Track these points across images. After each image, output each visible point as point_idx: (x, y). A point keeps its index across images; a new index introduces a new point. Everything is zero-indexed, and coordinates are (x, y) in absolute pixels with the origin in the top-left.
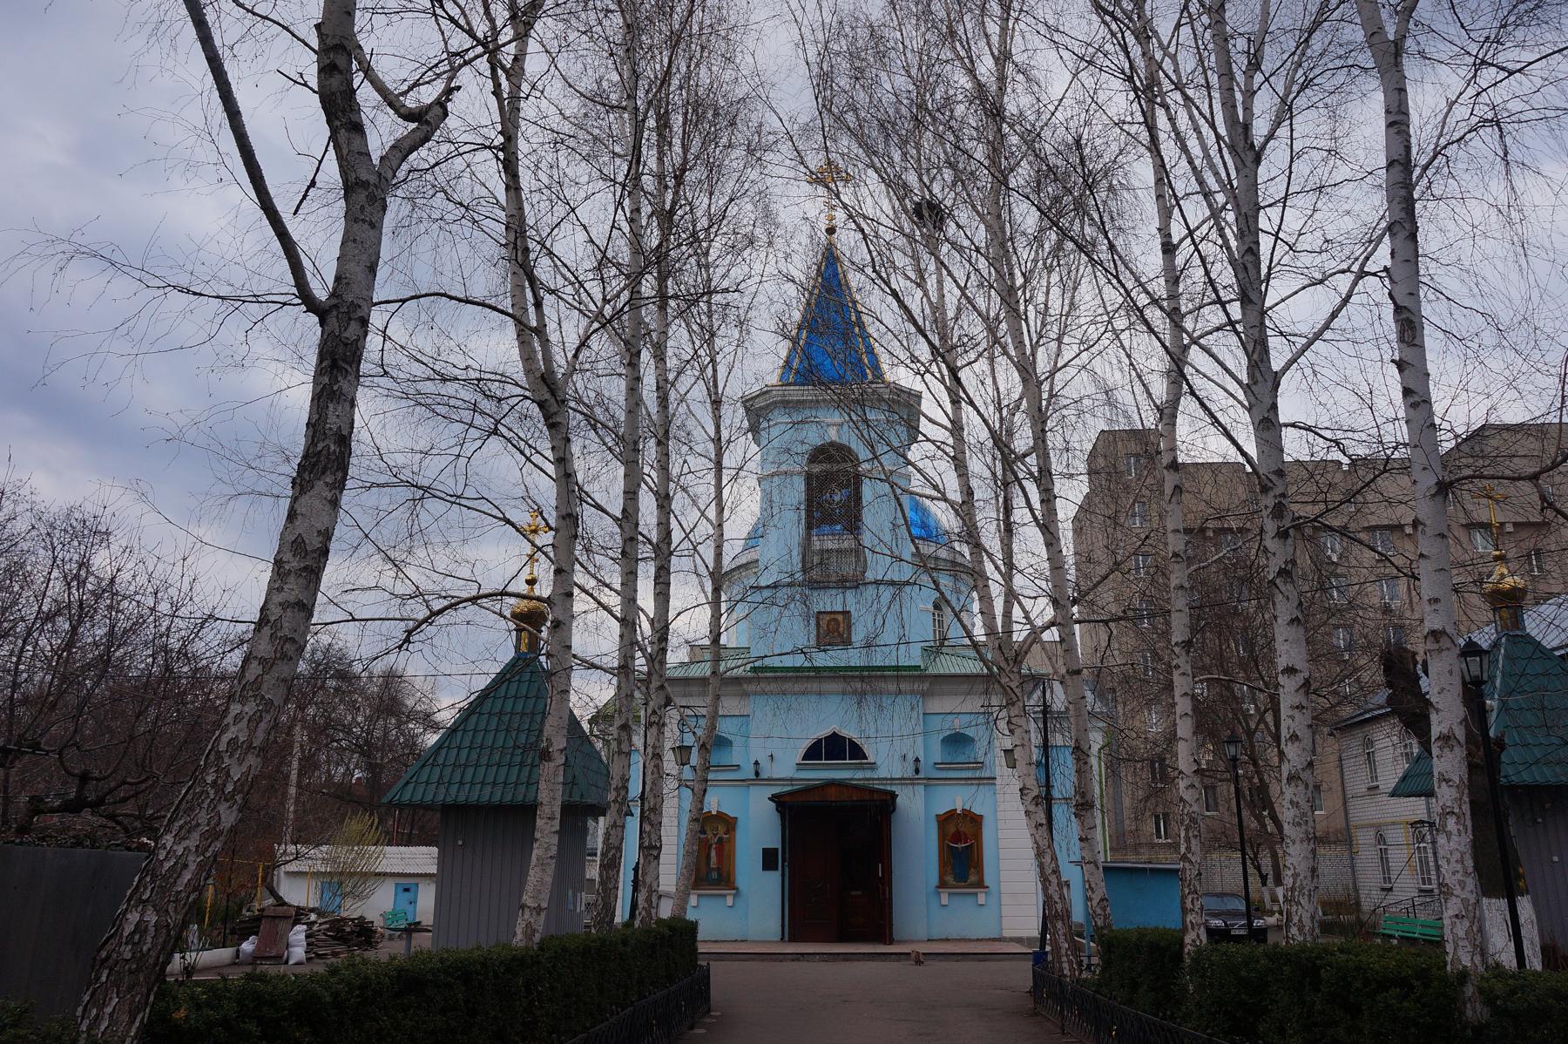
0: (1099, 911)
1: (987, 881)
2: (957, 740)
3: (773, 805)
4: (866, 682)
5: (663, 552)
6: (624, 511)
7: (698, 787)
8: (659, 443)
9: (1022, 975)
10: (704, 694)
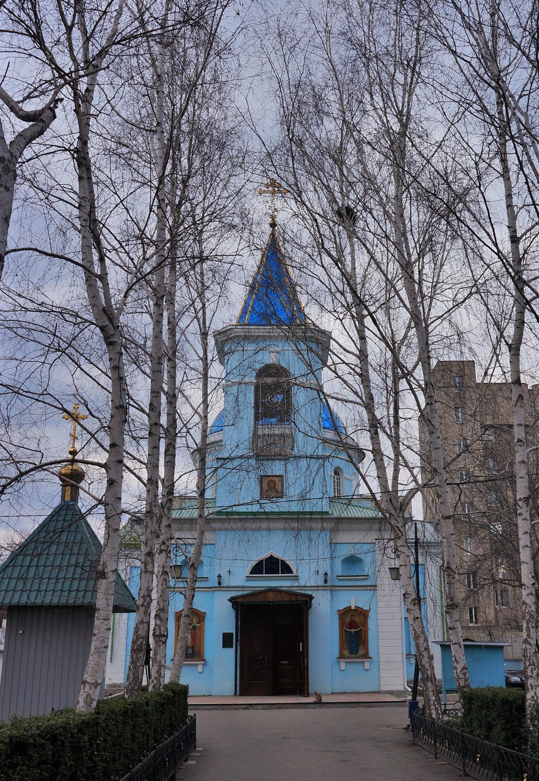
0: (461, 676)
1: (371, 654)
2: (352, 561)
3: (230, 604)
4: (300, 521)
5: (171, 434)
6: (151, 405)
7: (188, 593)
8: (169, 360)
9: (402, 717)
10: (191, 529)
